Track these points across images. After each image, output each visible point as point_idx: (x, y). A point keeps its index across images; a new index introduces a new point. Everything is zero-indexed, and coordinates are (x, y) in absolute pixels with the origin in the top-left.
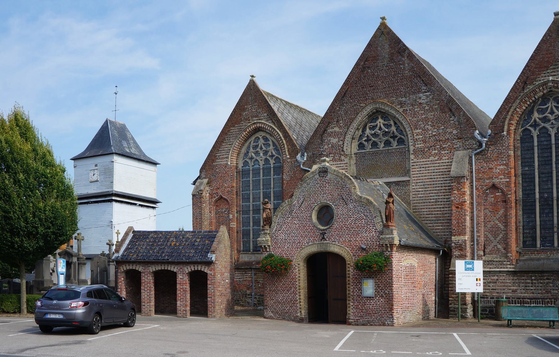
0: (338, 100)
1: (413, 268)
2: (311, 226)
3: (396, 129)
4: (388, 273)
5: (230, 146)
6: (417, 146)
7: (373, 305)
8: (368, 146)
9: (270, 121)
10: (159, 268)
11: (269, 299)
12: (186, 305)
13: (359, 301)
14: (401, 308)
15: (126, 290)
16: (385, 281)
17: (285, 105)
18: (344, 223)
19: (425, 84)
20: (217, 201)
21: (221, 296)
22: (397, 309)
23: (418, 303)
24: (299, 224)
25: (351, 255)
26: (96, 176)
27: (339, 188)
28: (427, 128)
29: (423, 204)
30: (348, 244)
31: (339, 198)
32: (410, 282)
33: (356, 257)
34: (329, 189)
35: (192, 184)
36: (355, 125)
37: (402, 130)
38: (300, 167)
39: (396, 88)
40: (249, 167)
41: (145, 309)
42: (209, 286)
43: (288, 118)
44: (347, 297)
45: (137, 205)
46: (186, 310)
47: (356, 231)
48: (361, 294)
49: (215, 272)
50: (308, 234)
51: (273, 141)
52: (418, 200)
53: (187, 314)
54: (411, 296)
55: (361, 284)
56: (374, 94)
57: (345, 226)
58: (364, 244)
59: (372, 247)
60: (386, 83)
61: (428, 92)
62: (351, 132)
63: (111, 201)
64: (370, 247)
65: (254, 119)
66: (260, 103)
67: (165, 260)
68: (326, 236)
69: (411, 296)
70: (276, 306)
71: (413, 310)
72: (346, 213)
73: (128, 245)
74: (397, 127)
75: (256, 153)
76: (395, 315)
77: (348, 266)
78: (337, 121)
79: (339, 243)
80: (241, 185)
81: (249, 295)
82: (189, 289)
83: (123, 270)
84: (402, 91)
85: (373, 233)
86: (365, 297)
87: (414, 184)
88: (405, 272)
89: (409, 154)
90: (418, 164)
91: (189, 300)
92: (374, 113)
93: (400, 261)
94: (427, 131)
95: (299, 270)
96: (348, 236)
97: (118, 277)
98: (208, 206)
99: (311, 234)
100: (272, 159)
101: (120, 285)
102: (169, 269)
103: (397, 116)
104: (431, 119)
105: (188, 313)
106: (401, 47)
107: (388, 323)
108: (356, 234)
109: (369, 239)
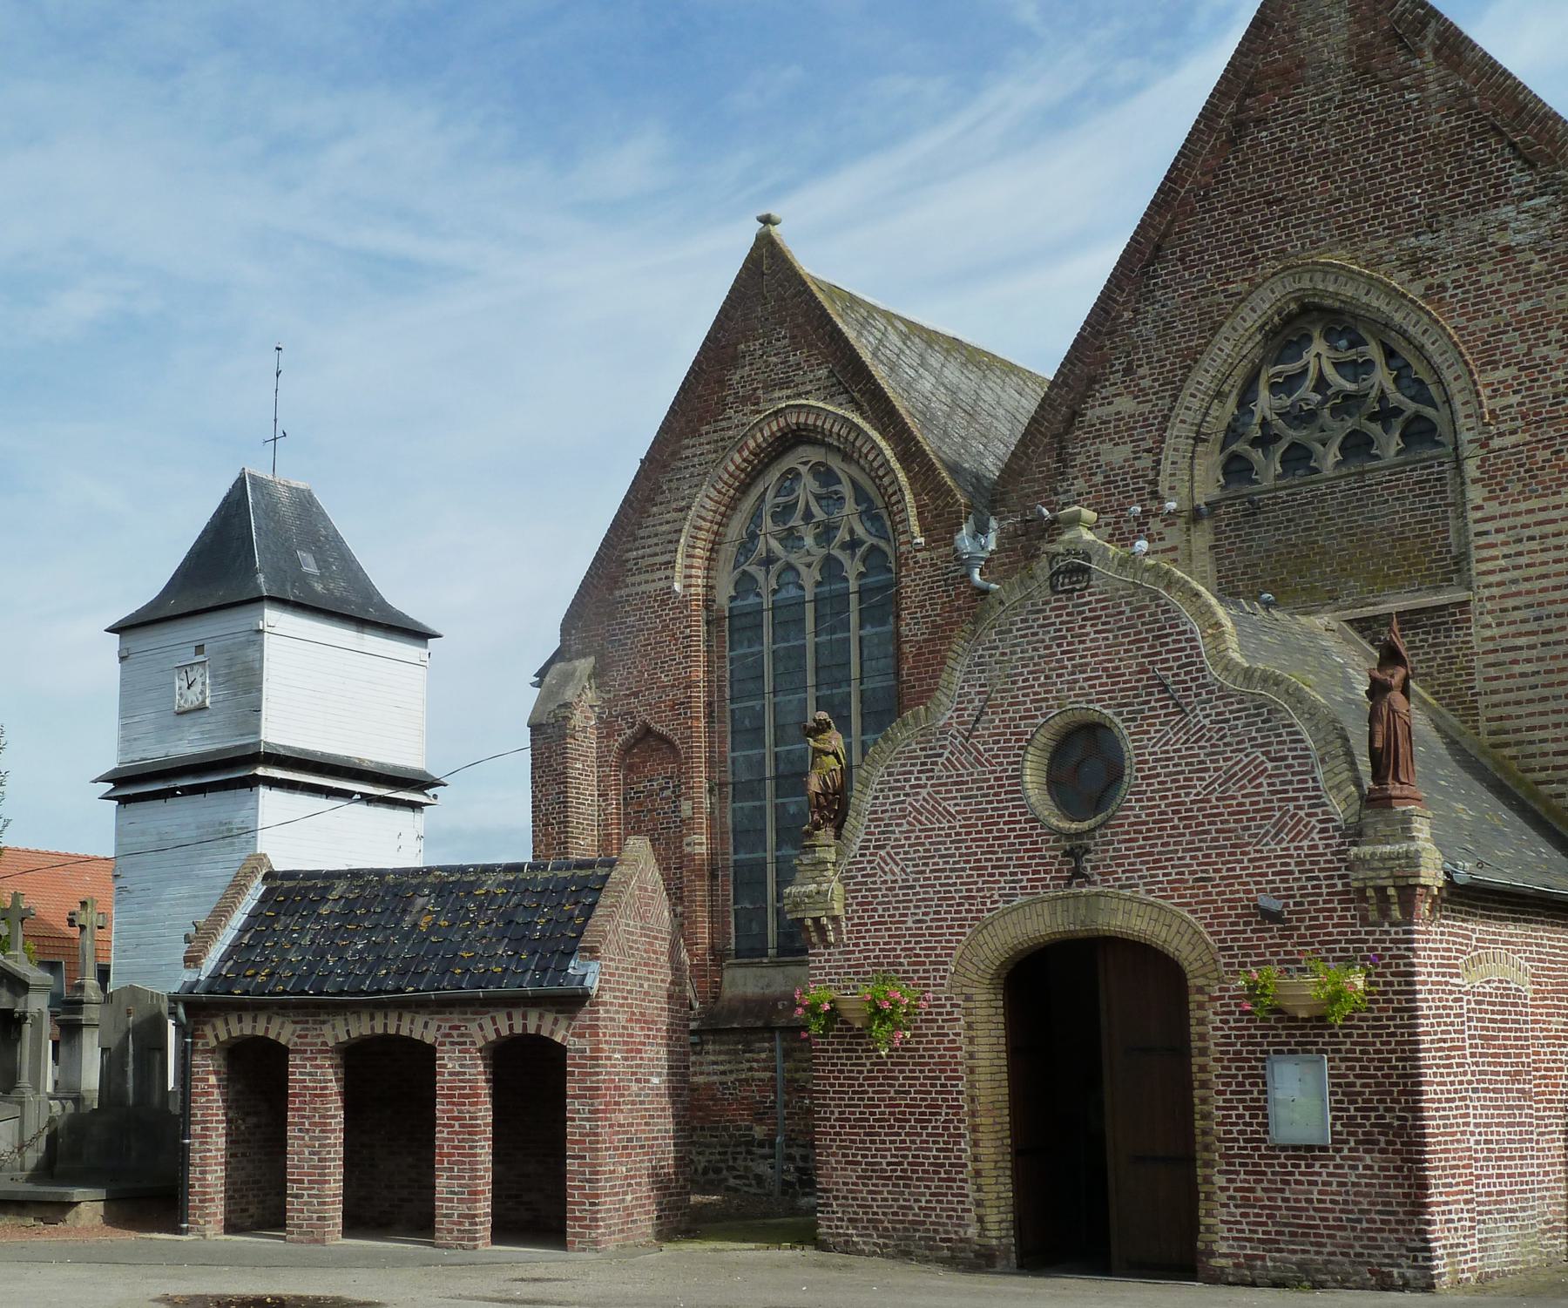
0: (1129, 278)
1: (1515, 1005)
2: (1019, 822)
3: (1396, 380)
4: (1396, 1026)
5: (681, 515)
6: (1496, 443)
7: (1325, 1184)
8: (1268, 467)
9: (842, 398)
10: (361, 1027)
11: (837, 1162)
12: (475, 1193)
13: (1254, 1165)
14: (1467, 1202)
15: (229, 1128)
16: (1382, 1068)
17: (905, 338)
18: (1174, 796)
19: (1526, 161)
20: (633, 746)
21: (625, 1148)
22: (1446, 1203)
23: (1546, 1174)
24: (964, 812)
25: (1207, 944)
26: (197, 688)
27: (1146, 640)
28: (1544, 358)
29: (1539, 707)
30: (1192, 896)
31: (1146, 687)
32: (1505, 1073)
33: (1235, 956)
34: (1099, 647)
35: (533, 684)
36: (1204, 377)
37: (1420, 382)
38: (969, 582)
39: (1386, 195)
40: (758, 600)
41: (302, 1211)
42: (572, 1105)
43: (919, 387)
44: (1198, 1147)
45: (357, 797)
46: (475, 1216)
47: (1229, 831)
48: (1267, 1132)
49: (599, 1042)
50: (1010, 859)
51: (854, 483)
52: (1511, 690)
53: (476, 1231)
54: (1510, 1141)
55: (1265, 1084)
56: (1288, 235)
57: (1178, 812)
58: (1273, 890)
59: (1311, 903)
60: (1343, 180)
61: (1542, 195)
62: (1188, 408)
63: (253, 782)
64: (1301, 904)
65: (777, 394)
66: (798, 326)
67: (387, 992)
68: (1089, 861)
69: (1510, 1141)
70: (870, 1192)
71: (1523, 1209)
72: (1179, 750)
73: (243, 930)
74: (1398, 369)
75: (786, 538)
76: (1441, 1236)
77: (1199, 997)
78: (1128, 371)
79: (1150, 892)
80: (728, 675)
81: (761, 1145)
82: (490, 1120)
83: (213, 1043)
84: (1418, 206)
85: (1315, 835)
86: (1284, 1148)
87: (1488, 619)
88: (1479, 1020)
89: (1463, 483)
90: (1504, 523)
91: (486, 1170)
92: (1289, 320)
93: (1449, 966)
94: (1541, 372)
95: (970, 1026)
96: (1192, 858)
97: (192, 1074)
98: (595, 770)
99: (1022, 858)
100: (853, 556)
101: (199, 1108)
102: (404, 1032)
103: (1398, 317)
104: (1558, 312)
105: (485, 1228)
106: (1403, 13)
107: (1402, 1276)
108: (1233, 846)
109: (1292, 867)
